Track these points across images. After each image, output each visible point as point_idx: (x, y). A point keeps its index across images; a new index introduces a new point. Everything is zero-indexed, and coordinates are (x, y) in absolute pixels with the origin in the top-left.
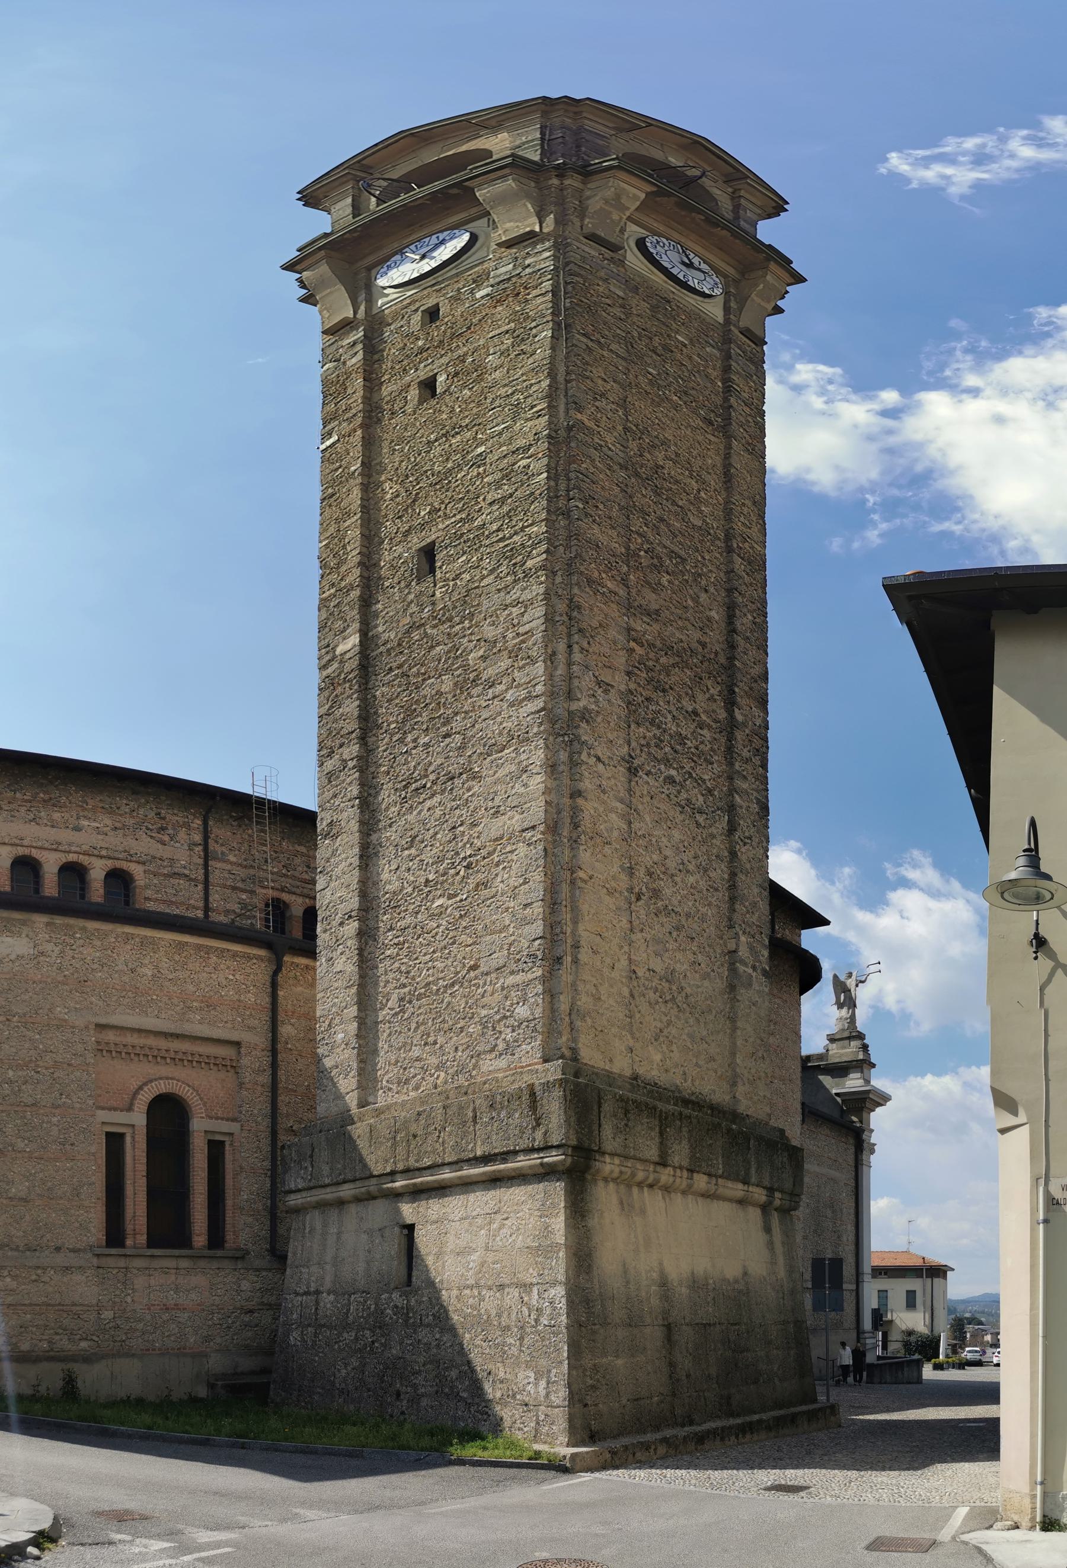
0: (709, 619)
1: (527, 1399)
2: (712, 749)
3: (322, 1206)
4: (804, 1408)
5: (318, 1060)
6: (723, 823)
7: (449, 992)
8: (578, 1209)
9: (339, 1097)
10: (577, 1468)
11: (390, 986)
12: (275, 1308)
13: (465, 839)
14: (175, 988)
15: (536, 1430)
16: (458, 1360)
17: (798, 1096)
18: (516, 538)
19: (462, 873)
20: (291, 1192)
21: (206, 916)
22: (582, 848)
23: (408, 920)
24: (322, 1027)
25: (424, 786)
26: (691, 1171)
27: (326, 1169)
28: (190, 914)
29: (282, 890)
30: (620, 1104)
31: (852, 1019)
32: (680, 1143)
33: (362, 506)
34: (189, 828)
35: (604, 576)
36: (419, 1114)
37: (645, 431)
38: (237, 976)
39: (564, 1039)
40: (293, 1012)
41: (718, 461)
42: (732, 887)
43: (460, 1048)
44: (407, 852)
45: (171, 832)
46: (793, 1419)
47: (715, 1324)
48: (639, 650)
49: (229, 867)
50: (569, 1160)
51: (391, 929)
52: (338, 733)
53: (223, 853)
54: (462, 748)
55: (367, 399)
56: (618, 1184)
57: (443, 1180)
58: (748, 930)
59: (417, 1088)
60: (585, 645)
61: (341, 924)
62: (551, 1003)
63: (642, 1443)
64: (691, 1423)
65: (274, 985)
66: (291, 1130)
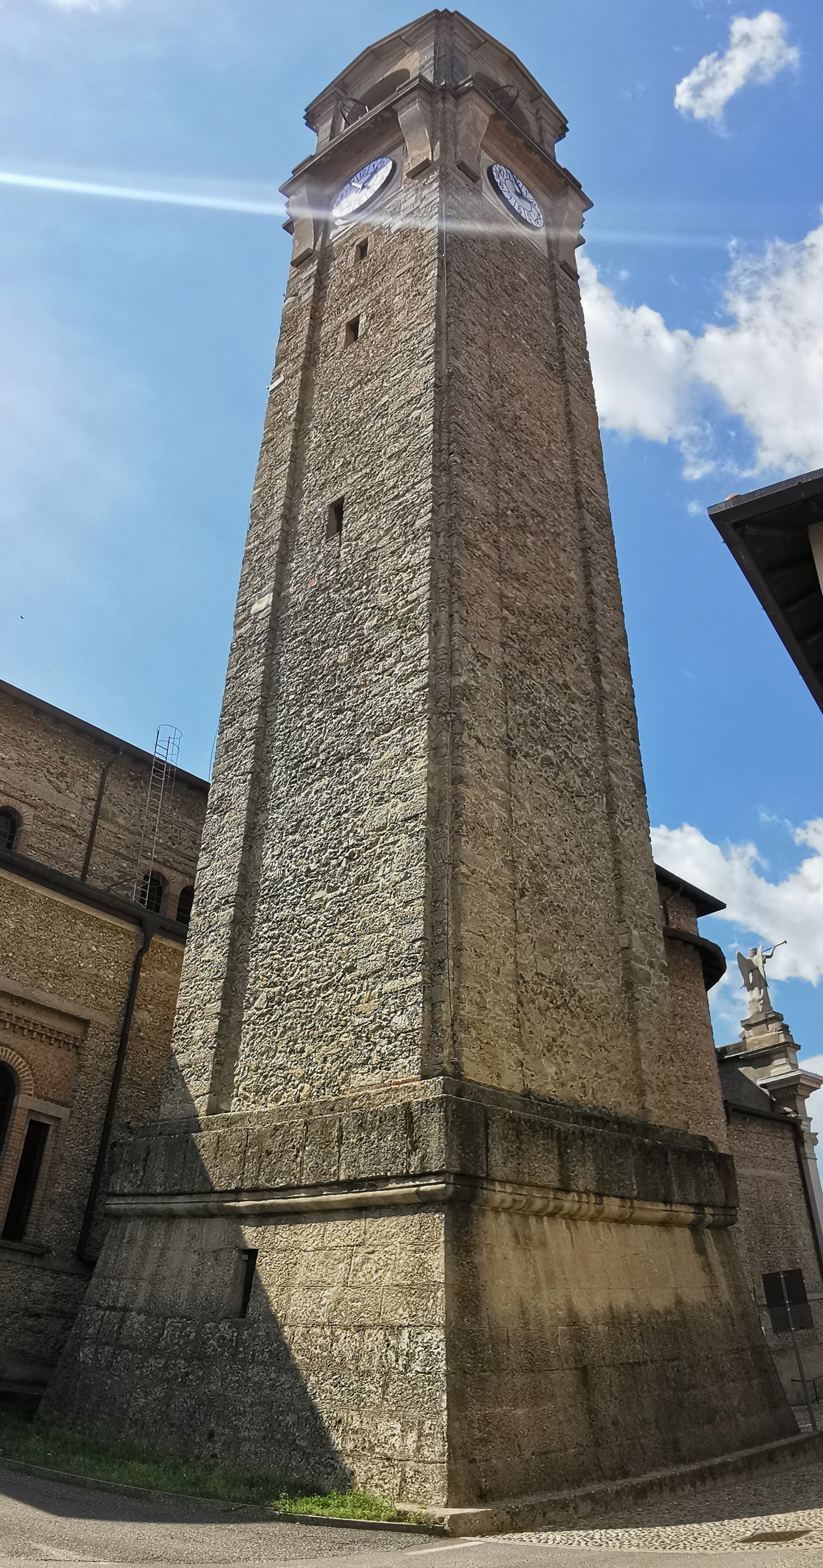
0: (569, 581)
1: (389, 1453)
2: (585, 725)
3: (149, 1216)
4: (783, 1442)
5: (170, 1055)
6: (601, 809)
7: (322, 995)
8: (462, 1245)
9: (188, 1099)
10: (461, 1531)
11: (260, 983)
12: (69, 1317)
13: (350, 826)
14: (34, 949)
15: (401, 1488)
16: (298, 1404)
17: (719, 1095)
18: (408, 495)
19: (343, 864)
20: (115, 1195)
21: (83, 877)
22: (463, 839)
23: (286, 912)
24: (179, 1019)
25: (314, 766)
26: (599, 1195)
27: (160, 1176)
28: (68, 872)
29: (164, 864)
30: (511, 1125)
31: (766, 999)
32: (583, 1166)
33: (292, 454)
34: (87, 779)
35: (479, 537)
36: (276, 1129)
37: (504, 379)
38: (101, 950)
39: (446, 1052)
40: (152, 998)
41: (561, 407)
42: (618, 876)
43: (330, 1059)
44: (291, 837)
45: (69, 780)
46: (770, 1456)
47: (645, 1362)
48: (512, 620)
49: (115, 830)
50: (451, 1188)
51: (268, 920)
52: (241, 699)
53: (113, 814)
54: (352, 726)
55: (310, 338)
56: (511, 1215)
57: (298, 1204)
58: (639, 922)
59: (276, 1100)
60: (465, 614)
61: (217, 909)
62: (432, 1012)
63: (555, 1502)
64: (626, 1474)
65: (137, 966)
66: (127, 1126)
